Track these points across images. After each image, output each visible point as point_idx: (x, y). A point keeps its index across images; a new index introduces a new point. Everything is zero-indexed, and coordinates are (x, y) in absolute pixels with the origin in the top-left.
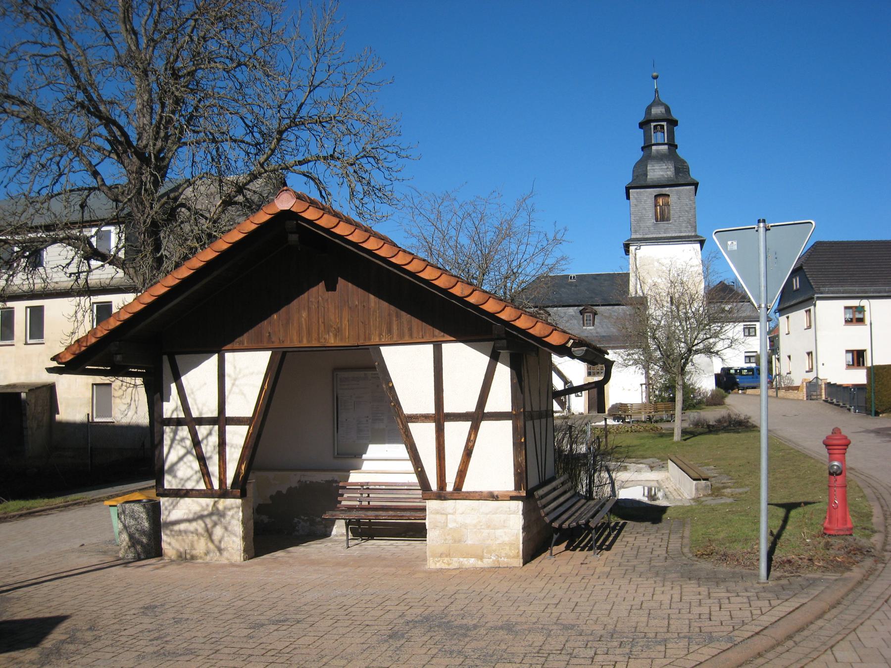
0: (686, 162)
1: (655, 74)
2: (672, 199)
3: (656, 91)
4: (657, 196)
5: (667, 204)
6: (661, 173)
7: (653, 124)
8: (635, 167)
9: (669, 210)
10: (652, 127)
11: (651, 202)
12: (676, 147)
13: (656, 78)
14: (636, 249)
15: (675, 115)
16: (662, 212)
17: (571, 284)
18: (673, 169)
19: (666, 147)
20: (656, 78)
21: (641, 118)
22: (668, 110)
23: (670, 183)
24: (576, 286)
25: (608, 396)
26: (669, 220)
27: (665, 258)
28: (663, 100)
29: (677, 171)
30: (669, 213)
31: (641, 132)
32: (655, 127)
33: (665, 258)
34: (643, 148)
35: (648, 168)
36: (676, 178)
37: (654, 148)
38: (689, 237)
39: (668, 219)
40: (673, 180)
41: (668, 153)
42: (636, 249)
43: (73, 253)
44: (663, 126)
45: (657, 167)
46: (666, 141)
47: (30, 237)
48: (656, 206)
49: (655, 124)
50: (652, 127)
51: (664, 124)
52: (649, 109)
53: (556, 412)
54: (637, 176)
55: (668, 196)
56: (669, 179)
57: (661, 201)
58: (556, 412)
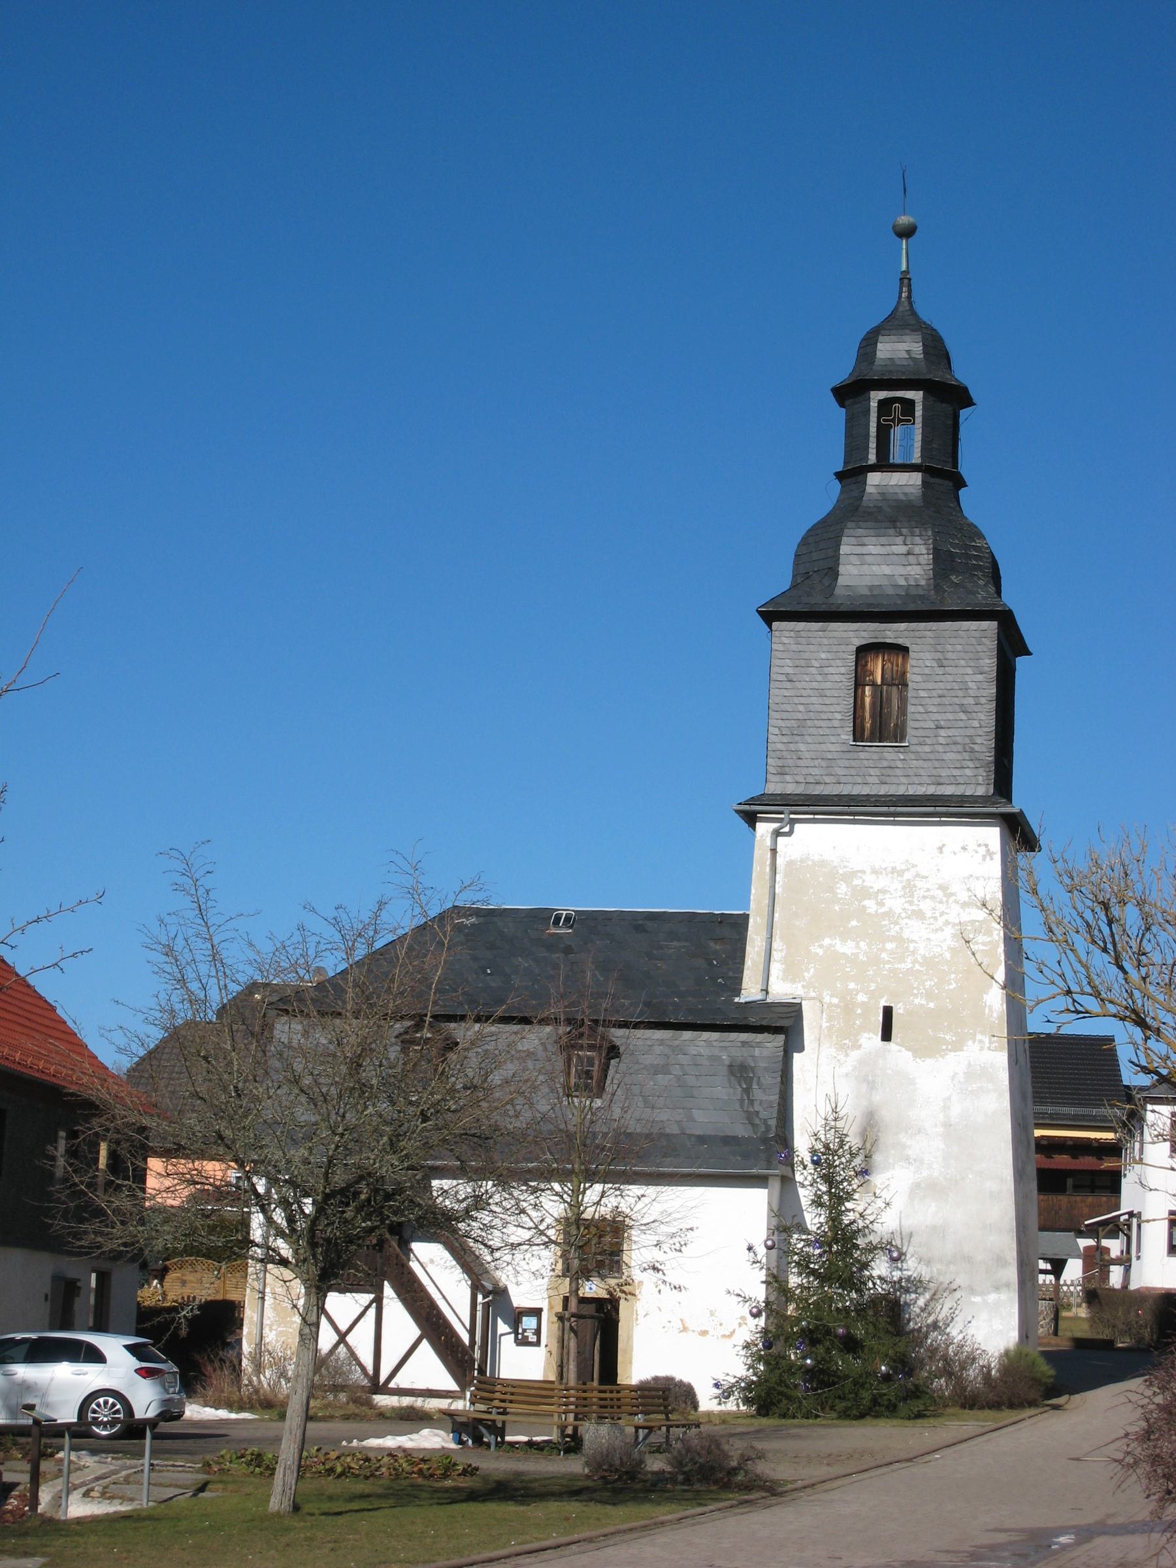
0: (981, 536)
1: (904, 220)
2: (919, 667)
3: (905, 279)
4: (864, 651)
5: (901, 682)
6: (887, 570)
7: (877, 396)
8: (804, 542)
9: (903, 701)
10: (874, 405)
11: (842, 670)
12: (960, 483)
13: (907, 233)
14: (777, 833)
15: (963, 372)
16: (880, 704)
17: (553, 944)
18: (927, 558)
19: (916, 478)
20: (907, 233)
21: (842, 371)
22: (936, 349)
23: (911, 607)
24: (568, 950)
25: (629, 1349)
26: (902, 739)
27: (875, 872)
28: (925, 313)
29: (943, 563)
30: (903, 711)
31: (840, 414)
32: (884, 405)
33: (875, 872)
34: (840, 476)
35: (844, 549)
36: (937, 588)
37: (874, 479)
38: (962, 800)
39: (899, 734)
40: (922, 597)
41: (920, 503)
42: (777, 833)
43: (556, 1215)
44: (882, 403)
45: (874, 547)
46: (916, 458)
47: (158, 1322)
48: (859, 684)
49: (883, 395)
50: (874, 405)
51: (916, 396)
52: (869, 343)
53: (465, 1406)
54: (807, 575)
55: (904, 650)
56: (909, 593)
57: (877, 668)
58: (465, 1406)
